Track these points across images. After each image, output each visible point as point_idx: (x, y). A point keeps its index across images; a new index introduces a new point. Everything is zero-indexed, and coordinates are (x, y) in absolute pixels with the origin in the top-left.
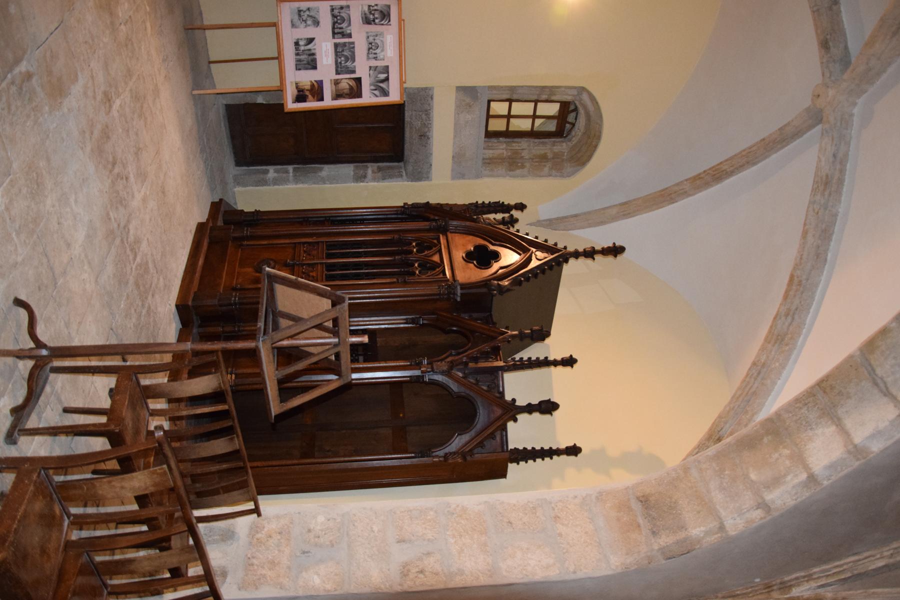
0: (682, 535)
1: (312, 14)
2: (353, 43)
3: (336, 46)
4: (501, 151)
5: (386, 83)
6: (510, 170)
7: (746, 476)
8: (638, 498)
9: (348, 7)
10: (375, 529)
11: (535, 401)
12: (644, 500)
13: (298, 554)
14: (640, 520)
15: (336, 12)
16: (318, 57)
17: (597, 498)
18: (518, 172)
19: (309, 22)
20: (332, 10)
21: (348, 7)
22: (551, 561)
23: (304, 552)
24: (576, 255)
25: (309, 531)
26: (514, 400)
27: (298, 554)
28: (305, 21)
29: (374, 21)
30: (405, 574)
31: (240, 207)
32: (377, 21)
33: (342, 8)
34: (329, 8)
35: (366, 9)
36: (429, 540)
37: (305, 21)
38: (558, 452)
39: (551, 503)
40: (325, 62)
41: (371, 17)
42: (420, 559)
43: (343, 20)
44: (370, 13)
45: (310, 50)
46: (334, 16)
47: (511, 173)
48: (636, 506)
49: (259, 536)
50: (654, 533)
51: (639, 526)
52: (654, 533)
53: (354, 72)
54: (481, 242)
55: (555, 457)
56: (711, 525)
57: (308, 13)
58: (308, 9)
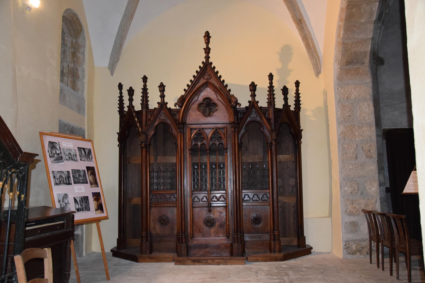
0: (368, 54)
1: (61, 199)
2: (72, 170)
3: (75, 183)
4: (69, 81)
5: (86, 150)
6: (79, 78)
7: (362, 23)
8: (346, 65)
9: (53, 172)
10: (351, 167)
11: (283, 97)
12: (348, 63)
13: (362, 196)
14: (355, 67)
15: (58, 181)
16: (83, 196)
17: (340, 81)
18: (80, 73)
19: (66, 202)
20: (57, 184)
21: (53, 172)
22: (366, 104)
23: (362, 194)
24: (207, 58)
25: (352, 193)
26: (158, 103)
27: (362, 196)
28: (66, 204)
29: (58, 154)
30: (370, 157)
31: (116, 246)
32: (58, 152)
33: (54, 177)
34: (56, 186)
35: (52, 159)
36: (357, 147)
37: (66, 204)
38: (145, 86)
39: (340, 99)
40: (83, 191)
41: (56, 156)
42: (365, 151)
43: (61, 176)
44: (54, 156)
45: (80, 201)
46: (60, 184)
47: (81, 77)
48: (350, 67)
49: (354, 212)
50: (363, 63)
51: (358, 68)
52: (363, 63)
53: (84, 171)
54: (195, 106)
55: (299, 92)
56: (370, 42)
57: (61, 202)
58: (59, 201)
